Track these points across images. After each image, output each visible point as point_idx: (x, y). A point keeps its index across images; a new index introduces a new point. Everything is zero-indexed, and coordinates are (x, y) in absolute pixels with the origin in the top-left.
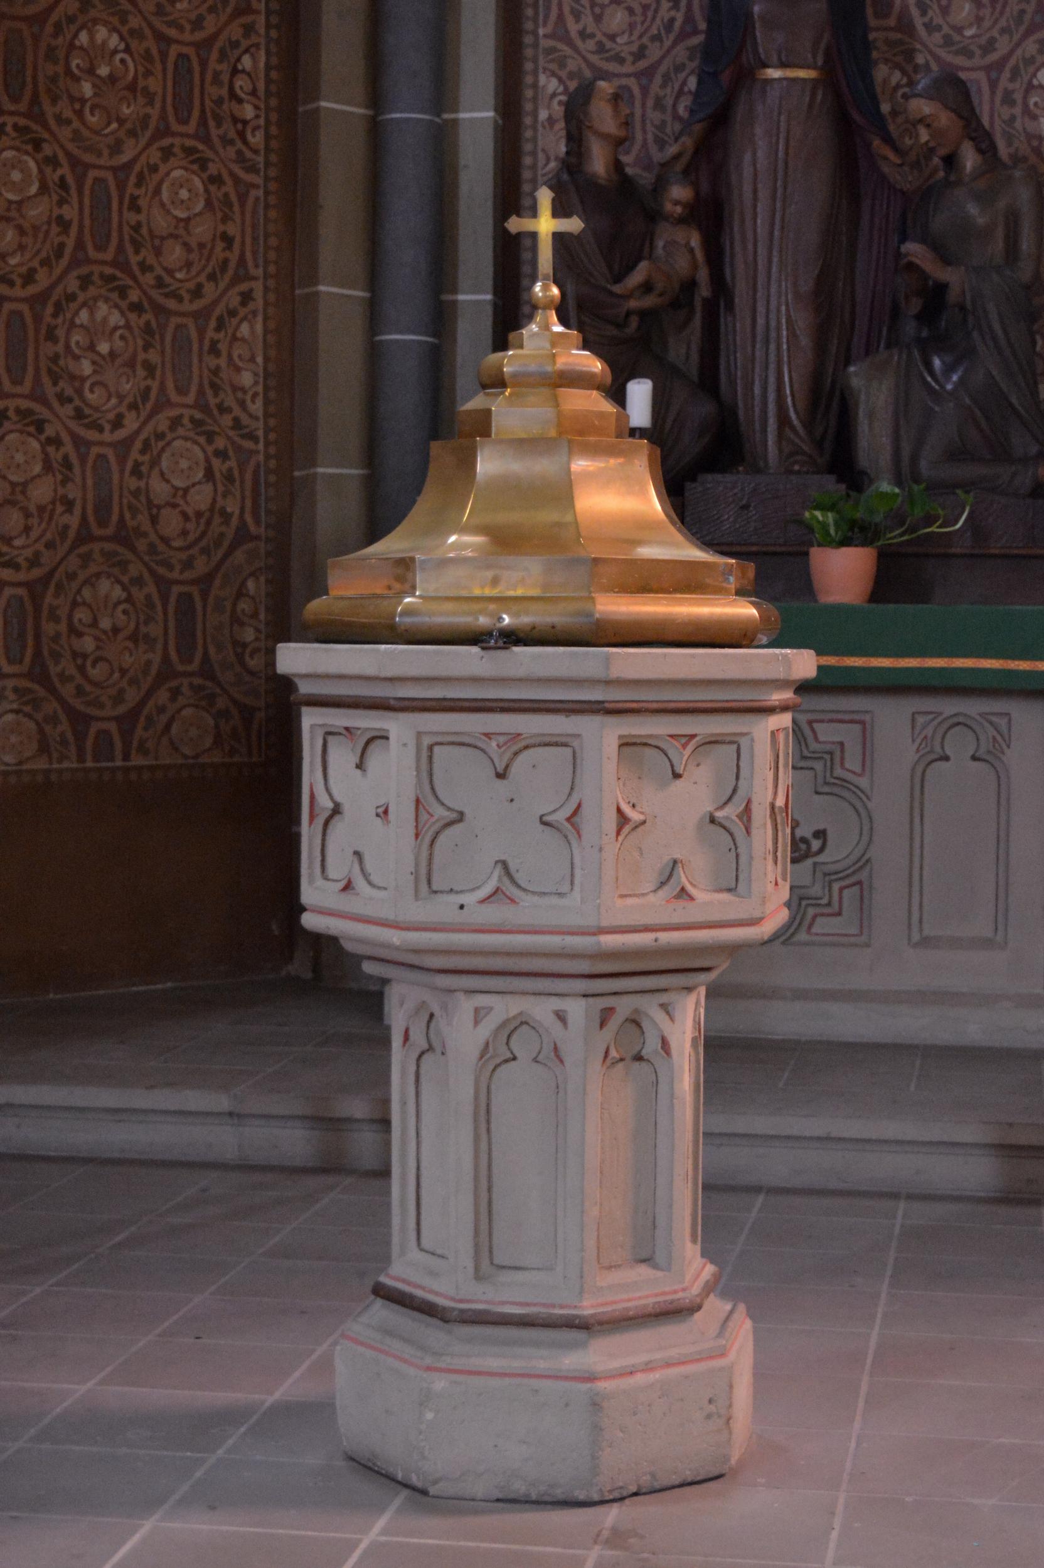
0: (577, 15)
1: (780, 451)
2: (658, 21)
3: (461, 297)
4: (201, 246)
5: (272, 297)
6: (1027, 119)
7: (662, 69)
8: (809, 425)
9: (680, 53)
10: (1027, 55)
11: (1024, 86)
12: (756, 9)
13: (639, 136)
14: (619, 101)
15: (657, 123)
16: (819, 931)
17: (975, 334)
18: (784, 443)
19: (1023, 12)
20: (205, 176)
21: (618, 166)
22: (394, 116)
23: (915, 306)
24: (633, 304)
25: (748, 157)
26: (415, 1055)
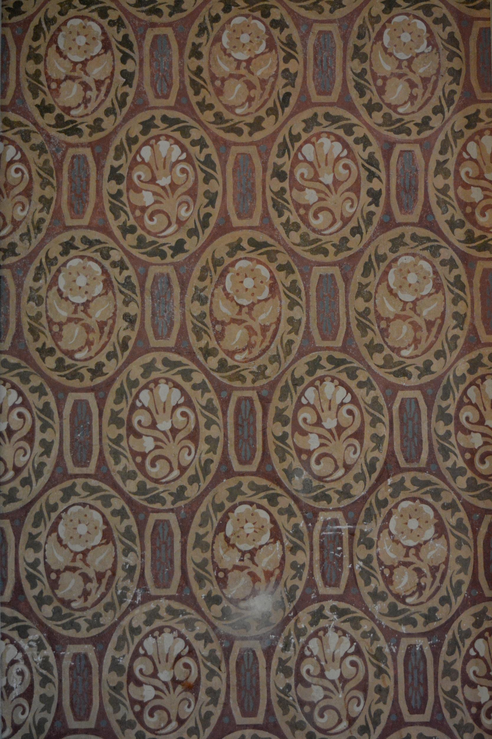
4: (263, 82)
20: (268, 21)
26: (339, 709)
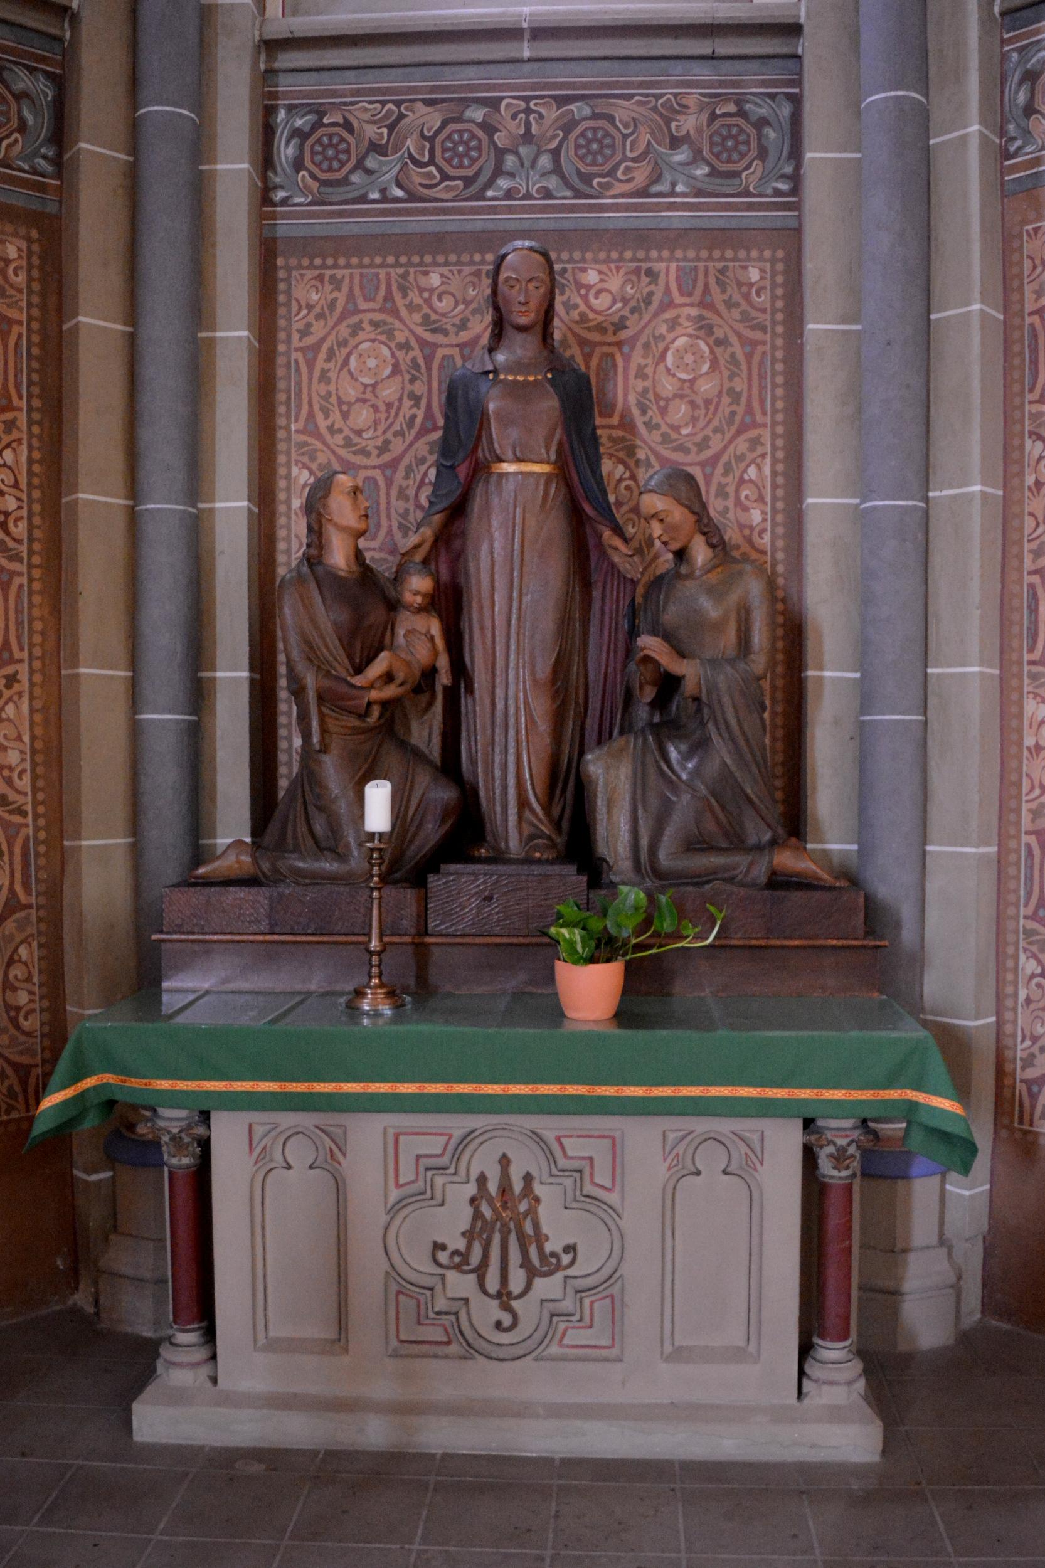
0: (326, 413)
1: (520, 833)
2: (401, 418)
3: (219, 674)
5: (37, 678)
6: (739, 510)
7: (405, 462)
8: (547, 808)
9: (422, 447)
10: (738, 453)
11: (736, 480)
12: (491, 406)
13: (384, 523)
14: (358, 493)
15: (401, 511)
16: (571, 1343)
17: (710, 725)
18: (524, 825)
19: (733, 413)
21: (358, 555)
22: (149, 506)
23: (649, 693)
24: (374, 695)
25: (485, 548)
